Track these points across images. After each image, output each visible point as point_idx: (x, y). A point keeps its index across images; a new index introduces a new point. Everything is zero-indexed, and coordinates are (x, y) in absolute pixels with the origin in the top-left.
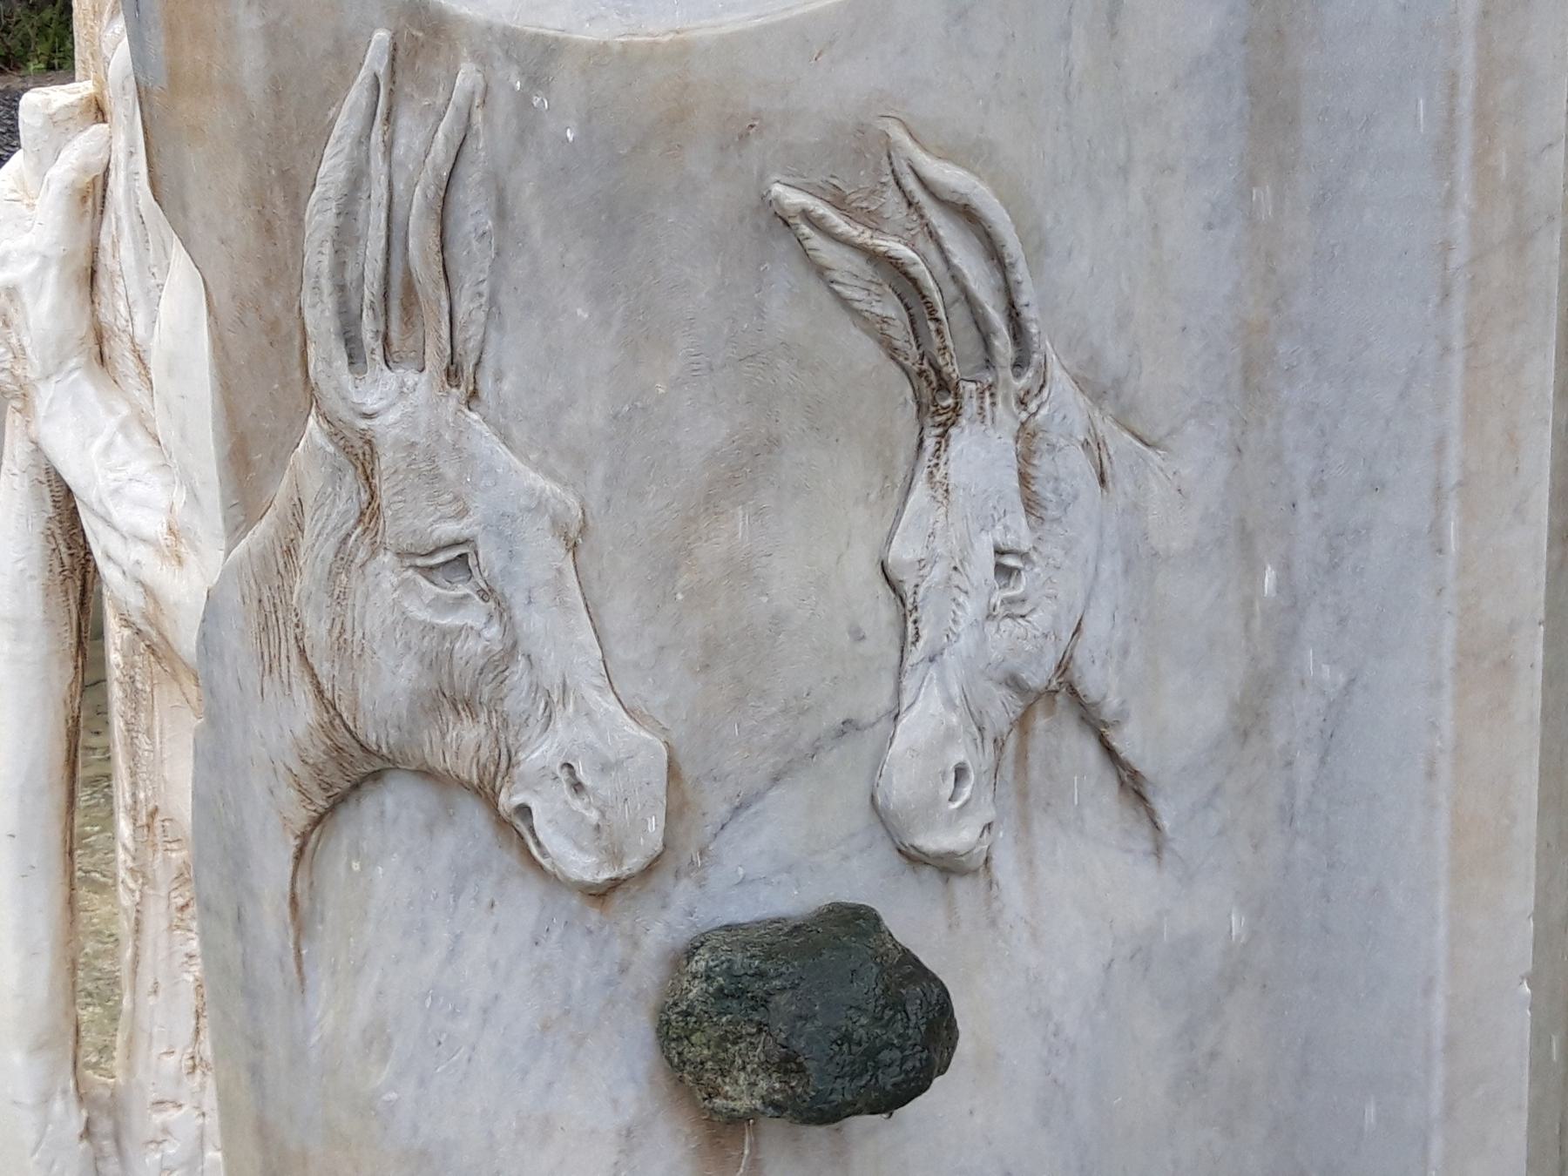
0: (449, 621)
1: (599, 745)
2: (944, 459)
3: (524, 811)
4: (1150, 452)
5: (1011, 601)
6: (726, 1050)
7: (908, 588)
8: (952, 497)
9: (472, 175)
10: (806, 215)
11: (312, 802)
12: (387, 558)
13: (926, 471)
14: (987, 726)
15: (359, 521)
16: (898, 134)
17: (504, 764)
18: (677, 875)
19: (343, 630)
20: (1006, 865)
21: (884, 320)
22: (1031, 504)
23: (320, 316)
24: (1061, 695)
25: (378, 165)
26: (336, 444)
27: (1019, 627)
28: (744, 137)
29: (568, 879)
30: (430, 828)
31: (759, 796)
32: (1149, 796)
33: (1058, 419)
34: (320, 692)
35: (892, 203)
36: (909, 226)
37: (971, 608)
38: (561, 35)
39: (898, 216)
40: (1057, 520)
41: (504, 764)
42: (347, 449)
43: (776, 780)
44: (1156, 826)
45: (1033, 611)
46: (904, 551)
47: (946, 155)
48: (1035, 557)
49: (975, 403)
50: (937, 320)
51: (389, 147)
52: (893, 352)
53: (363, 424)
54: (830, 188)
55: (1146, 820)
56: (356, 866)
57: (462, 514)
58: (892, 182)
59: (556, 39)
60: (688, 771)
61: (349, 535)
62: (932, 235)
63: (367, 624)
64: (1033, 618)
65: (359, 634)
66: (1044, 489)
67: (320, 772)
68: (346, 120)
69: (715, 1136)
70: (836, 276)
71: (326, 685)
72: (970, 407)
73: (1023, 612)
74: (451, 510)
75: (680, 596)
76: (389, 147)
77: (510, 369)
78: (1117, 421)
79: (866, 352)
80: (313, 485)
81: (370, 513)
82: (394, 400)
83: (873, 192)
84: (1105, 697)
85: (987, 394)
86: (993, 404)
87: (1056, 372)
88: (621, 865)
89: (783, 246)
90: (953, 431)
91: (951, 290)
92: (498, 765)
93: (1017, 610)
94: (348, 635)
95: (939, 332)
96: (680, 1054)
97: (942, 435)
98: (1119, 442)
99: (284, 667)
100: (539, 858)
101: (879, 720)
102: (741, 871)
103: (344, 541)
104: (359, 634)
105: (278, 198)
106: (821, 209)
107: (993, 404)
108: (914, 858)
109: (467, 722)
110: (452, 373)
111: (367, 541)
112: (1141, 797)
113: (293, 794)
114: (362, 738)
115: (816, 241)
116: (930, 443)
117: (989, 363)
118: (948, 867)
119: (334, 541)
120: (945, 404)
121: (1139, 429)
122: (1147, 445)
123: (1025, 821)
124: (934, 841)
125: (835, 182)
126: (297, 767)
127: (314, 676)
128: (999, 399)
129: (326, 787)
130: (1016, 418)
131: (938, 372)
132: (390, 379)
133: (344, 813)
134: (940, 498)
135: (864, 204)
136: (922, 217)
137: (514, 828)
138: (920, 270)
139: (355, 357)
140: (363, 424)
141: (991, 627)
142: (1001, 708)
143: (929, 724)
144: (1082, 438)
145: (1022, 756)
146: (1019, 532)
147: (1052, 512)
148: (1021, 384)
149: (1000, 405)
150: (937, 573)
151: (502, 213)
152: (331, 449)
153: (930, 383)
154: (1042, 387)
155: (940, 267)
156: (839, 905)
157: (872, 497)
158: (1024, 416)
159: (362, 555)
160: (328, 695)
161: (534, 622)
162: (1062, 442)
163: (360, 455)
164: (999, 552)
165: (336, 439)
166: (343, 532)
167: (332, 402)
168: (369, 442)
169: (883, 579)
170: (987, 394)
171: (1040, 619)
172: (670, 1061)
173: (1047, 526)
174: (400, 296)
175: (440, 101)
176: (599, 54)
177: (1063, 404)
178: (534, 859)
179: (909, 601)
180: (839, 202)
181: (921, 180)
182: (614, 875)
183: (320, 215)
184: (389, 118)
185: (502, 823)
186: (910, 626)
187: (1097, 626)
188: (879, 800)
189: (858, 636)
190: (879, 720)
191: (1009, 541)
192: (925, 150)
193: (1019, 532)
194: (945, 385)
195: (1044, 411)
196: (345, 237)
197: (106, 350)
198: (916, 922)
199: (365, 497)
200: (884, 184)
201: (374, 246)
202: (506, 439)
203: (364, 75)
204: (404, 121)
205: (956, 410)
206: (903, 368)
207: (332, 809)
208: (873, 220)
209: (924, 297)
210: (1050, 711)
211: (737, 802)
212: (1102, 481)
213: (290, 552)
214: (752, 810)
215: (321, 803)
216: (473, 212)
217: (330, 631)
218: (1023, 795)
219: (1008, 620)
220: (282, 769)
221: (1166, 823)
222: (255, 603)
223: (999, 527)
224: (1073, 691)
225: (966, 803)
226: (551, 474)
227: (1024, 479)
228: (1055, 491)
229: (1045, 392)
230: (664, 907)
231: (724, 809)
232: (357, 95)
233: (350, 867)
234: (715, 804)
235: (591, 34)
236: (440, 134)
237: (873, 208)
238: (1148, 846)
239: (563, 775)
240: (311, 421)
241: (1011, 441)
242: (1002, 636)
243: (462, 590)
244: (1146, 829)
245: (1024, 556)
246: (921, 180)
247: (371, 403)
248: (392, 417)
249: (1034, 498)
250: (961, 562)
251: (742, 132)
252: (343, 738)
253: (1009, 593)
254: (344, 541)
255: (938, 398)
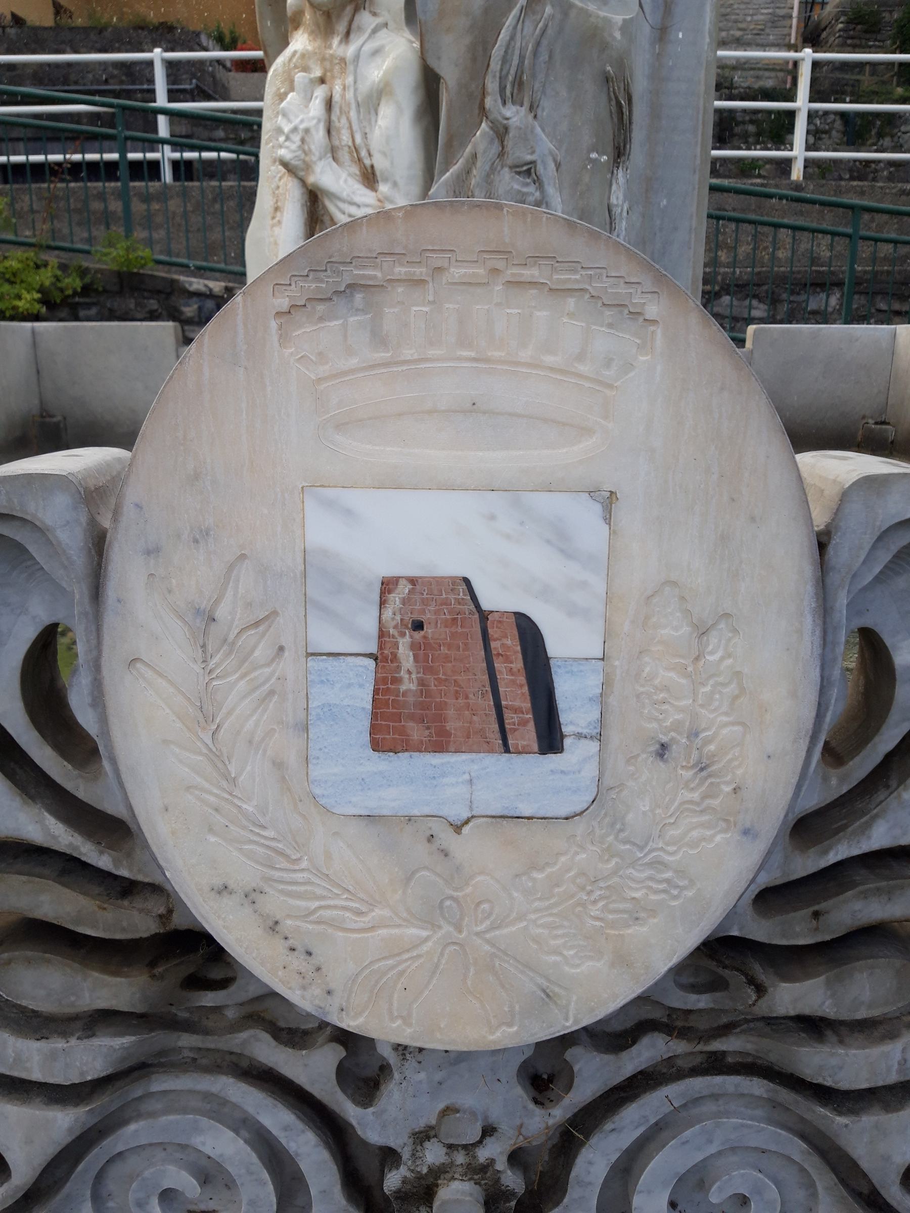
0: (525, 190)
9: (545, 42)
12: (506, 169)
23: (492, 85)
25: (518, 35)
51: (522, 30)
53: (505, 122)
57: (533, 153)
68: (510, 21)
74: (530, 151)
76: (522, 30)
77: (546, 107)
80: (481, 148)
81: (502, 154)
82: (515, 115)
110: (531, 108)
119: (490, 164)
132: (514, 108)
140: (505, 122)
151: (550, 57)
152: (491, 132)
159: (499, 168)
163: (501, 132)
167: (494, 115)
174: (519, 83)
175: (539, 17)
183: (497, 52)
184: (523, 22)
196: (505, 60)
201: (515, 62)
202: (543, 130)
203: (518, 6)
204: (527, 23)
213: (468, 172)
216: (544, 56)
232: (515, 12)
236: (335, 912)
243: (528, 181)
247: (508, 114)
248: (514, 119)
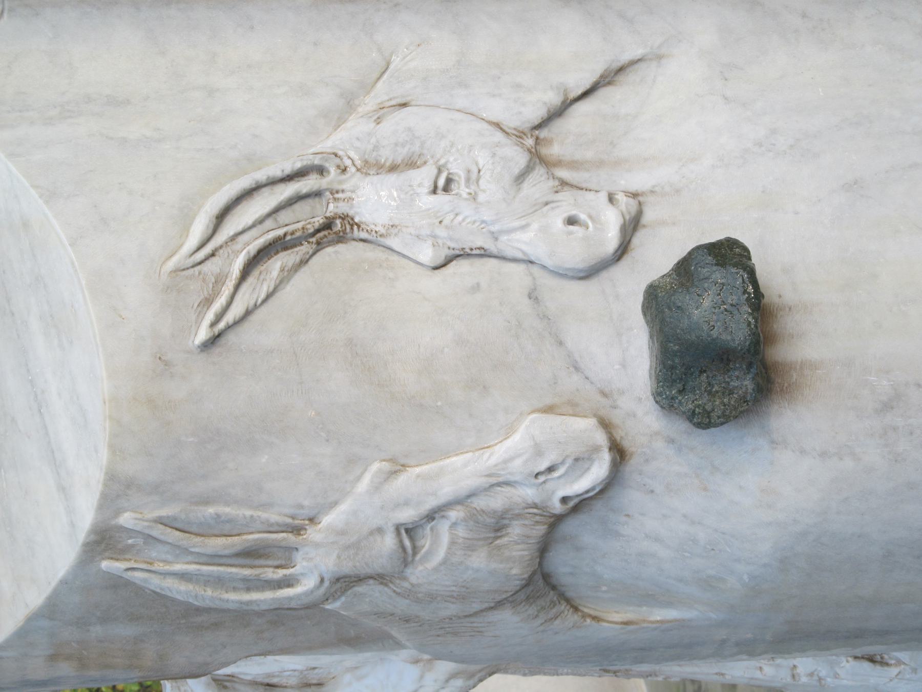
1: (524, 457)
2: (373, 227)
3: (564, 500)
4: (392, 67)
5: (468, 180)
6: (717, 392)
7: (452, 252)
8: (397, 222)
10: (213, 324)
11: (563, 612)
13: (379, 238)
14: (545, 199)
15: (386, 585)
16: (171, 264)
17: (535, 511)
18: (615, 407)
19: (452, 597)
20: (639, 180)
21: (282, 270)
22: (411, 164)
24: (536, 142)
26: (339, 597)
27: (486, 176)
28: (167, 364)
29: (608, 477)
30: (578, 549)
31: (570, 355)
32: (619, 64)
33: (358, 144)
34: (491, 608)
35: (211, 267)
36: (226, 255)
37: (467, 210)
38: (104, 470)
39: (220, 262)
40: (423, 144)
41: (535, 511)
42: (343, 591)
43: (561, 343)
44: (639, 60)
45: (477, 164)
46: (427, 254)
47: (186, 230)
48: (442, 162)
49: (341, 204)
50: (285, 235)
52: (304, 262)
53: (327, 584)
54: (199, 309)
55: (636, 66)
56: (604, 588)
58: (199, 267)
59: (107, 473)
60: (548, 401)
61: (394, 591)
62: (234, 238)
63: (447, 583)
64: (481, 163)
65: (454, 588)
66: (401, 154)
67: (543, 608)
69: (782, 390)
70: (252, 303)
71: (486, 605)
72: (343, 208)
73: (476, 171)
75: (439, 404)
78: (368, 93)
79: (302, 279)
83: (204, 280)
84: (545, 103)
85: (336, 196)
86: (343, 191)
87: (327, 145)
88: (601, 446)
89: (231, 338)
90: (356, 220)
91: (269, 223)
92: (535, 514)
93: (474, 176)
94: (455, 594)
95: (292, 233)
96: (719, 417)
97: (359, 226)
98: (382, 92)
99: (479, 625)
100: (595, 492)
101: (531, 274)
102: (617, 367)
103: (398, 594)
104: (454, 588)
105: (199, 619)
106: (210, 316)
107: (343, 191)
108: (623, 250)
109: (510, 530)
110: (297, 530)
111: (398, 581)
112: (621, 70)
113: (557, 622)
114: (518, 588)
115: (230, 317)
116: (363, 235)
117: (318, 194)
118: (632, 227)
120: (339, 226)
121: (375, 75)
122: (387, 69)
123: (618, 163)
124: (611, 239)
125: (196, 305)
126: (540, 621)
127: (482, 611)
128: (340, 187)
129: (553, 604)
130: (353, 175)
131: (318, 231)
133: (570, 594)
134: (396, 230)
135: (211, 286)
136: (221, 247)
137: (579, 505)
138: (253, 248)
139: (287, 582)
141: (482, 198)
142: (538, 185)
143: (543, 233)
144: (372, 125)
145: (574, 165)
146: (423, 177)
147: (416, 148)
148: (333, 170)
149: (344, 187)
150: (441, 232)
153: (325, 236)
154: (336, 155)
155: (254, 232)
156: (643, 306)
157: (391, 275)
158: (353, 169)
160: (492, 605)
161: (447, 490)
162: (373, 140)
164: (434, 191)
165: (336, 596)
166: (393, 595)
168: (338, 580)
169: (444, 269)
170: (336, 196)
171: (483, 158)
172: (722, 424)
173: (425, 151)
176: (113, 449)
177: (350, 138)
178: (596, 494)
179: (458, 252)
180: (208, 302)
181: (199, 248)
182: (607, 450)
183: (208, 595)
185: (576, 509)
186: (474, 252)
187: (496, 109)
188: (582, 275)
189: (476, 288)
190: (531, 274)
191: (428, 184)
192: (182, 245)
193: (423, 177)
194: (328, 225)
195: (352, 154)
196: (219, 582)
197: (315, 682)
198: (658, 257)
199: (371, 581)
200: (200, 273)
205: (344, 217)
206: (314, 253)
207: (568, 601)
208: (220, 280)
209: (270, 244)
210: (549, 142)
211: (572, 369)
212: (404, 105)
214: (578, 359)
215: (563, 606)
217: (453, 603)
218: (600, 164)
219: (481, 182)
220: (542, 628)
221: (639, 52)
222: (439, 638)
223: (419, 190)
224: (539, 126)
225: (590, 217)
226: (359, 478)
227: (393, 168)
228: (403, 146)
229: (340, 153)
230: (635, 416)
231: (576, 377)
233: (605, 592)
234: (571, 382)
235: (104, 455)
237: (213, 280)
238: (654, 64)
239: (542, 478)
240: (328, 607)
241: (368, 179)
242: (491, 189)
244: (642, 65)
245: (440, 171)
246: (199, 248)
249: (406, 161)
250: (437, 218)
251: (163, 364)
252: (522, 596)
253: (463, 182)
254: (398, 594)
255: (333, 231)
